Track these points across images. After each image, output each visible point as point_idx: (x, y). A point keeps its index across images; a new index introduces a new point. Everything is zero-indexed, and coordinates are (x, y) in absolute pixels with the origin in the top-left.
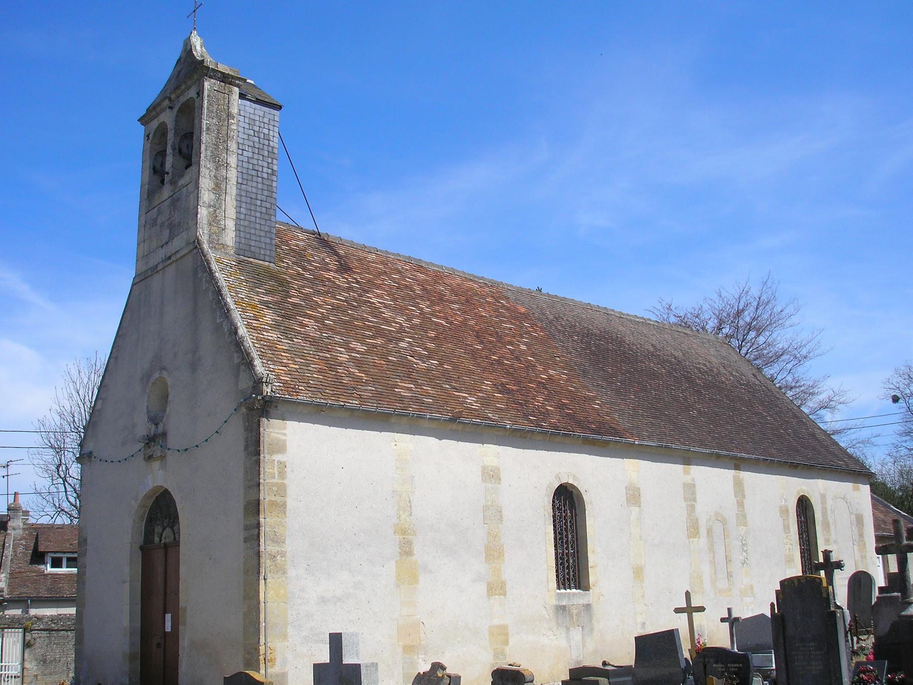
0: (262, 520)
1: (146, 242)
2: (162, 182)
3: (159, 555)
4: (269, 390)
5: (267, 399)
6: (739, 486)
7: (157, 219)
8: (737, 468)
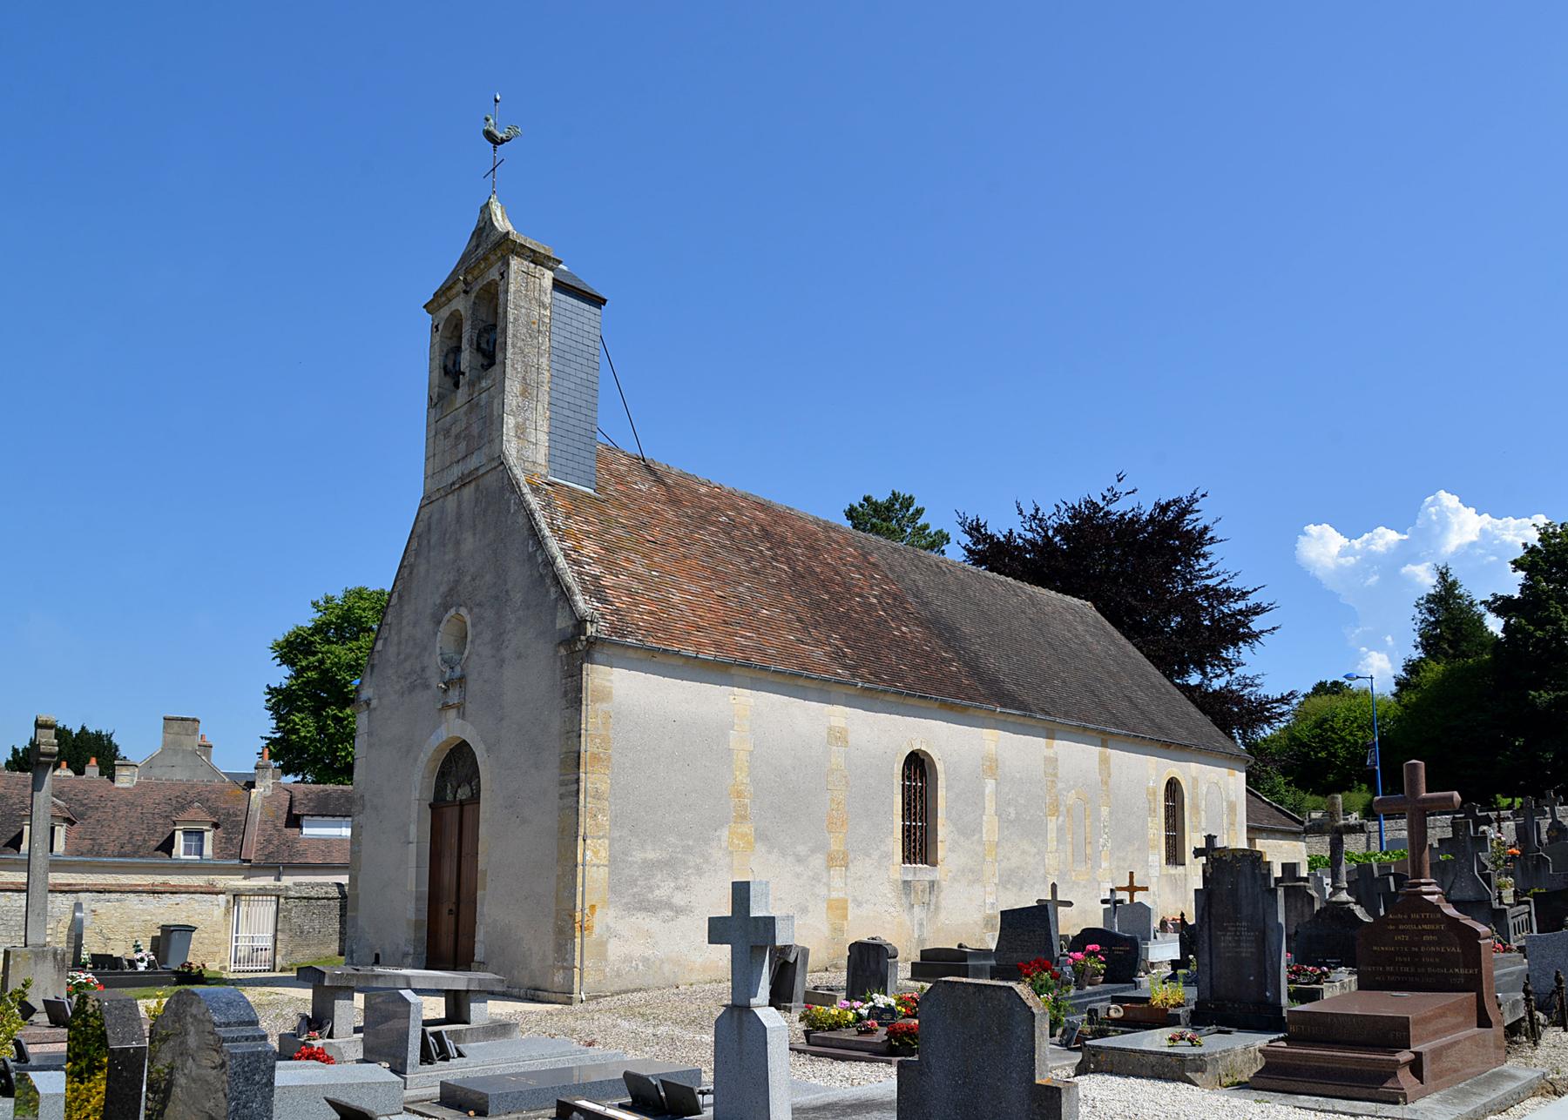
0: (582, 776)
1: (436, 456)
2: (457, 385)
3: (451, 815)
4: (594, 630)
5: (592, 640)
6: (1104, 761)
7: (450, 429)
8: (1104, 744)
